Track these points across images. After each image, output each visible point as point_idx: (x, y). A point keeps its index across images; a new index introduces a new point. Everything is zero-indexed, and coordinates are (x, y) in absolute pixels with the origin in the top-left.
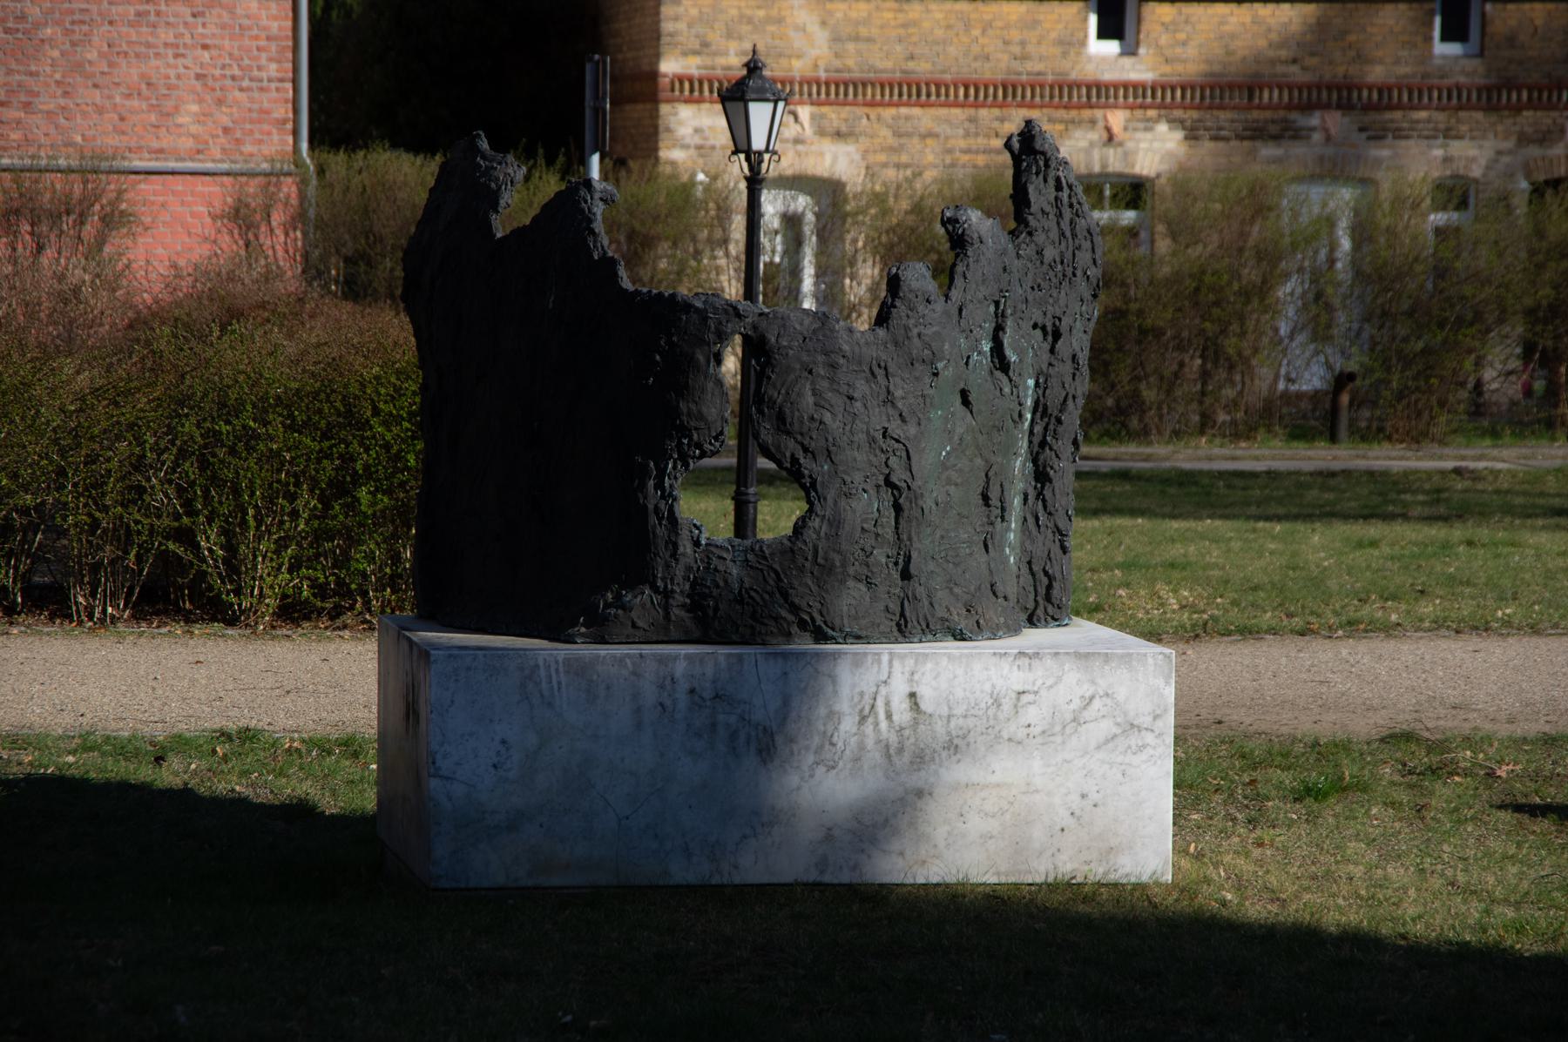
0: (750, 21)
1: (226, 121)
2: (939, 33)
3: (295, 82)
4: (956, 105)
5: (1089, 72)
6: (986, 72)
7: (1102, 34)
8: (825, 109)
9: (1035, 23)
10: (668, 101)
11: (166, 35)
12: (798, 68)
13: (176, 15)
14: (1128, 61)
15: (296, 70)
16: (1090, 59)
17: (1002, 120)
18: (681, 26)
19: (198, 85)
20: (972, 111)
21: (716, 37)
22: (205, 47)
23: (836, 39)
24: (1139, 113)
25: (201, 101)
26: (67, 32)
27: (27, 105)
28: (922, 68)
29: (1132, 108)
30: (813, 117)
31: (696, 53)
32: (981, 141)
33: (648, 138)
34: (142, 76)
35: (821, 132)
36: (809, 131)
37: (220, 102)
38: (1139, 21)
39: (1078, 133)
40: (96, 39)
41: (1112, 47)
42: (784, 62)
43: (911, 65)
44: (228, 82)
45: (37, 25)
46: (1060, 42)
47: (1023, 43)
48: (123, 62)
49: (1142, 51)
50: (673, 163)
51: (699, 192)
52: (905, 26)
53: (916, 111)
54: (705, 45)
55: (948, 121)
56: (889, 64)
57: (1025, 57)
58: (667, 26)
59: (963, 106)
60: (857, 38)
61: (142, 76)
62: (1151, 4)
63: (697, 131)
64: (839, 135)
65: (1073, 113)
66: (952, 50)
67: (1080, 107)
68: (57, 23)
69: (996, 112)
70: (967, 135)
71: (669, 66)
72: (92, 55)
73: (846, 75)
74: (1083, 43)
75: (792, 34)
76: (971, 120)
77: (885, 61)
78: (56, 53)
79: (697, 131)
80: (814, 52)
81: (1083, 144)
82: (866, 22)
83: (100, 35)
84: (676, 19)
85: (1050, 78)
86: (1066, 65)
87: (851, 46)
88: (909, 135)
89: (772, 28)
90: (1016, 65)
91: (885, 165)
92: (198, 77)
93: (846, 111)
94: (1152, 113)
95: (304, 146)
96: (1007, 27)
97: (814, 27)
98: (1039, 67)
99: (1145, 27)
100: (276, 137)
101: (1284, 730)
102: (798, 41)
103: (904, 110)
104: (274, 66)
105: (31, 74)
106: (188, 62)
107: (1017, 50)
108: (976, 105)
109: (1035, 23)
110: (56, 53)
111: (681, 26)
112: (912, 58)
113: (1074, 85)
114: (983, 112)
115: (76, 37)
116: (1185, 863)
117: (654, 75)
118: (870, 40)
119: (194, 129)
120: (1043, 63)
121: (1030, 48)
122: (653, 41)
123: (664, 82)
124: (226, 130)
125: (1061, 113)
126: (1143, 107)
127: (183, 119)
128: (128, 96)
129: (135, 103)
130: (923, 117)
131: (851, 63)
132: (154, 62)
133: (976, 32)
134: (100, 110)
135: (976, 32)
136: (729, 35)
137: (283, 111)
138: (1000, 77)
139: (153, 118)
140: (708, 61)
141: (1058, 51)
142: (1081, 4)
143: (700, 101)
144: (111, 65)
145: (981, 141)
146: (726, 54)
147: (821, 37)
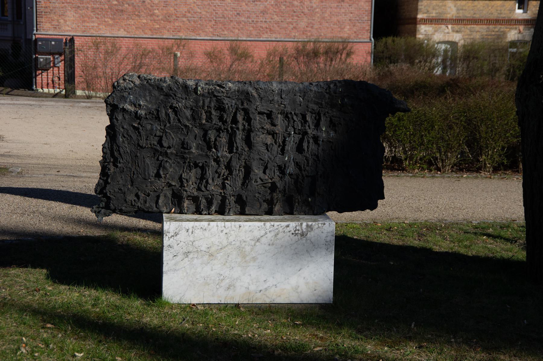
0: (438, 6)
1: (355, 30)
2: (481, 8)
3: (371, 21)
4: (484, 25)
5: (516, 17)
6: (492, 17)
7: (519, 8)
8: (455, 26)
9: (504, 6)
10: (419, 24)
11: (343, 11)
12: (449, 16)
13: (216, 3)
14: (525, 14)
15: (371, 18)
16: (516, 14)
17: (495, 28)
18: (423, 7)
19: (349, 22)
20: (488, 26)
21: (430, 9)
22: (351, 13)
23: (458, 10)
24: (527, 26)
25: (350, 26)
26: (321, 10)
27: (312, 27)
28: (477, 16)
29: (525, 25)
30: (452, 28)
31: (426, 13)
32: (490, 33)
33: (414, 33)
34: (337, 20)
35: (453, 31)
36: (450, 31)
37: (354, 26)
38: (528, 5)
39: (512, 31)
40: (328, 12)
41: (521, 11)
42: (445, 15)
43: (475, 15)
44: (356, 21)
45: (315, 9)
46: (509, 10)
47: (501, 10)
48: (333, 16)
49: (528, 12)
50: (419, 38)
51: (424, 45)
52: (474, 6)
53: (475, 26)
54: (428, 11)
55: (482, 28)
56: (469, 15)
57: (501, 14)
58: (419, 7)
59: (486, 25)
60: (462, 10)
61: (337, 20)
62: (531, 1)
63: (425, 31)
64: (457, 32)
65: (512, 26)
66: (484, 12)
67: (513, 25)
68: (319, 8)
69: (494, 26)
70: (487, 31)
71: (420, 16)
72: (326, 15)
73: (459, 18)
74: (515, 10)
75: (448, 9)
76: (488, 28)
77: (468, 15)
78: (319, 15)
79: (425, 31)
80: (453, 13)
81: (513, 33)
82: (464, 6)
83: (329, 11)
84: (422, 5)
85: (507, 18)
86: (510, 15)
87: (461, 11)
88: (473, 32)
89: (443, 7)
90: (499, 15)
91: (467, 38)
92: (350, 20)
93: (459, 26)
94: (530, 26)
95: (372, 35)
96: (497, 7)
97: (453, 7)
98: (504, 16)
99: (529, 6)
100: (366, 34)
101: (28, 154)
102: (449, 10)
103: (472, 26)
104: (366, 17)
105: (313, 20)
106: (348, 16)
107: (499, 12)
108: (489, 25)
109: (504, 6)
110: (319, 15)
111: (423, 7)
112: (475, 14)
113: (512, 20)
114: (491, 26)
115: (323, 11)
116: (277, 208)
117: (416, 18)
118: (465, 10)
119: (348, 32)
120: (505, 14)
121: (502, 11)
122: (416, 11)
123: (418, 20)
124: (355, 32)
125: (509, 26)
126: (528, 25)
127: (346, 30)
128: (334, 25)
129: (335, 26)
130: (477, 27)
131: (461, 15)
132: (340, 17)
133: (490, 8)
134: (328, 28)
135: (490, 8)
136: (433, 9)
137: (368, 28)
138: (495, 18)
139: (339, 29)
140: (428, 15)
141: (509, 12)
142: (514, 1)
143: (426, 24)
144: (331, 17)
145: (490, 33)
146: (432, 13)
147: (454, 9)
